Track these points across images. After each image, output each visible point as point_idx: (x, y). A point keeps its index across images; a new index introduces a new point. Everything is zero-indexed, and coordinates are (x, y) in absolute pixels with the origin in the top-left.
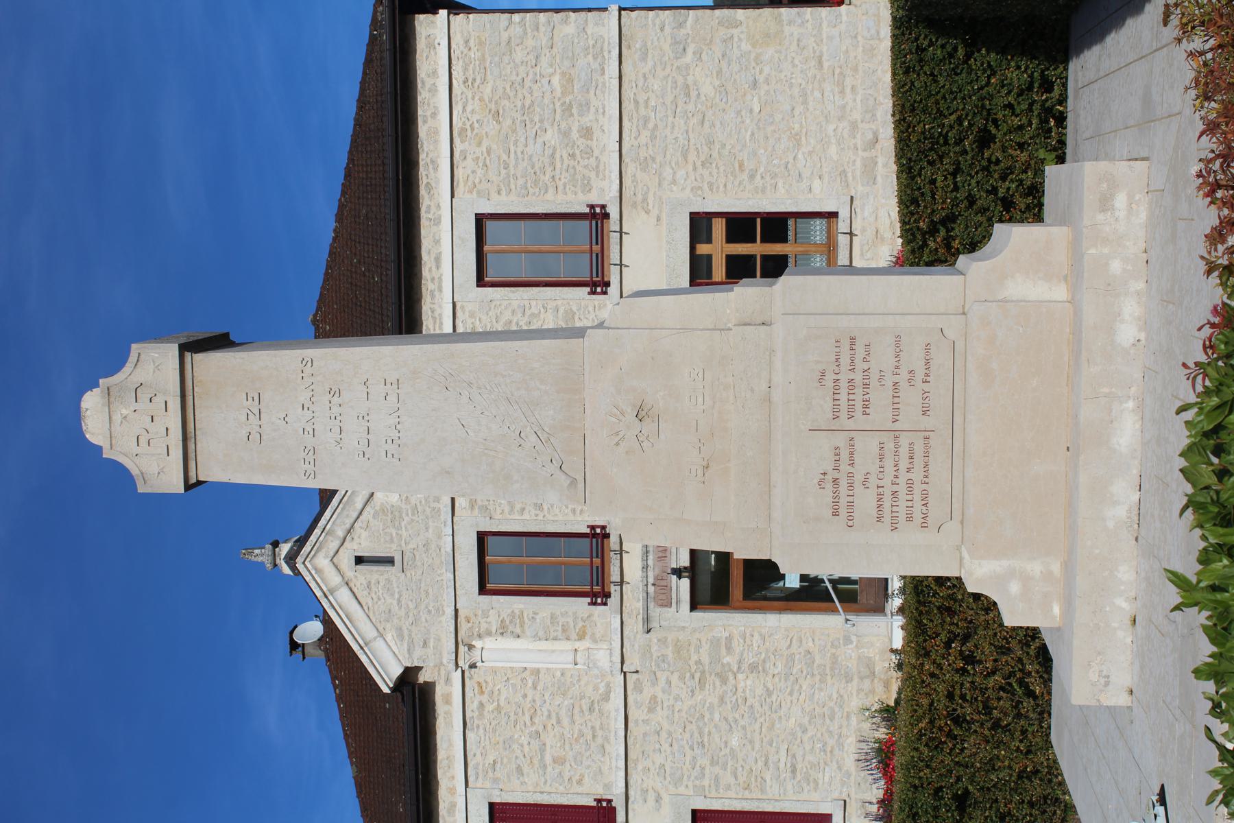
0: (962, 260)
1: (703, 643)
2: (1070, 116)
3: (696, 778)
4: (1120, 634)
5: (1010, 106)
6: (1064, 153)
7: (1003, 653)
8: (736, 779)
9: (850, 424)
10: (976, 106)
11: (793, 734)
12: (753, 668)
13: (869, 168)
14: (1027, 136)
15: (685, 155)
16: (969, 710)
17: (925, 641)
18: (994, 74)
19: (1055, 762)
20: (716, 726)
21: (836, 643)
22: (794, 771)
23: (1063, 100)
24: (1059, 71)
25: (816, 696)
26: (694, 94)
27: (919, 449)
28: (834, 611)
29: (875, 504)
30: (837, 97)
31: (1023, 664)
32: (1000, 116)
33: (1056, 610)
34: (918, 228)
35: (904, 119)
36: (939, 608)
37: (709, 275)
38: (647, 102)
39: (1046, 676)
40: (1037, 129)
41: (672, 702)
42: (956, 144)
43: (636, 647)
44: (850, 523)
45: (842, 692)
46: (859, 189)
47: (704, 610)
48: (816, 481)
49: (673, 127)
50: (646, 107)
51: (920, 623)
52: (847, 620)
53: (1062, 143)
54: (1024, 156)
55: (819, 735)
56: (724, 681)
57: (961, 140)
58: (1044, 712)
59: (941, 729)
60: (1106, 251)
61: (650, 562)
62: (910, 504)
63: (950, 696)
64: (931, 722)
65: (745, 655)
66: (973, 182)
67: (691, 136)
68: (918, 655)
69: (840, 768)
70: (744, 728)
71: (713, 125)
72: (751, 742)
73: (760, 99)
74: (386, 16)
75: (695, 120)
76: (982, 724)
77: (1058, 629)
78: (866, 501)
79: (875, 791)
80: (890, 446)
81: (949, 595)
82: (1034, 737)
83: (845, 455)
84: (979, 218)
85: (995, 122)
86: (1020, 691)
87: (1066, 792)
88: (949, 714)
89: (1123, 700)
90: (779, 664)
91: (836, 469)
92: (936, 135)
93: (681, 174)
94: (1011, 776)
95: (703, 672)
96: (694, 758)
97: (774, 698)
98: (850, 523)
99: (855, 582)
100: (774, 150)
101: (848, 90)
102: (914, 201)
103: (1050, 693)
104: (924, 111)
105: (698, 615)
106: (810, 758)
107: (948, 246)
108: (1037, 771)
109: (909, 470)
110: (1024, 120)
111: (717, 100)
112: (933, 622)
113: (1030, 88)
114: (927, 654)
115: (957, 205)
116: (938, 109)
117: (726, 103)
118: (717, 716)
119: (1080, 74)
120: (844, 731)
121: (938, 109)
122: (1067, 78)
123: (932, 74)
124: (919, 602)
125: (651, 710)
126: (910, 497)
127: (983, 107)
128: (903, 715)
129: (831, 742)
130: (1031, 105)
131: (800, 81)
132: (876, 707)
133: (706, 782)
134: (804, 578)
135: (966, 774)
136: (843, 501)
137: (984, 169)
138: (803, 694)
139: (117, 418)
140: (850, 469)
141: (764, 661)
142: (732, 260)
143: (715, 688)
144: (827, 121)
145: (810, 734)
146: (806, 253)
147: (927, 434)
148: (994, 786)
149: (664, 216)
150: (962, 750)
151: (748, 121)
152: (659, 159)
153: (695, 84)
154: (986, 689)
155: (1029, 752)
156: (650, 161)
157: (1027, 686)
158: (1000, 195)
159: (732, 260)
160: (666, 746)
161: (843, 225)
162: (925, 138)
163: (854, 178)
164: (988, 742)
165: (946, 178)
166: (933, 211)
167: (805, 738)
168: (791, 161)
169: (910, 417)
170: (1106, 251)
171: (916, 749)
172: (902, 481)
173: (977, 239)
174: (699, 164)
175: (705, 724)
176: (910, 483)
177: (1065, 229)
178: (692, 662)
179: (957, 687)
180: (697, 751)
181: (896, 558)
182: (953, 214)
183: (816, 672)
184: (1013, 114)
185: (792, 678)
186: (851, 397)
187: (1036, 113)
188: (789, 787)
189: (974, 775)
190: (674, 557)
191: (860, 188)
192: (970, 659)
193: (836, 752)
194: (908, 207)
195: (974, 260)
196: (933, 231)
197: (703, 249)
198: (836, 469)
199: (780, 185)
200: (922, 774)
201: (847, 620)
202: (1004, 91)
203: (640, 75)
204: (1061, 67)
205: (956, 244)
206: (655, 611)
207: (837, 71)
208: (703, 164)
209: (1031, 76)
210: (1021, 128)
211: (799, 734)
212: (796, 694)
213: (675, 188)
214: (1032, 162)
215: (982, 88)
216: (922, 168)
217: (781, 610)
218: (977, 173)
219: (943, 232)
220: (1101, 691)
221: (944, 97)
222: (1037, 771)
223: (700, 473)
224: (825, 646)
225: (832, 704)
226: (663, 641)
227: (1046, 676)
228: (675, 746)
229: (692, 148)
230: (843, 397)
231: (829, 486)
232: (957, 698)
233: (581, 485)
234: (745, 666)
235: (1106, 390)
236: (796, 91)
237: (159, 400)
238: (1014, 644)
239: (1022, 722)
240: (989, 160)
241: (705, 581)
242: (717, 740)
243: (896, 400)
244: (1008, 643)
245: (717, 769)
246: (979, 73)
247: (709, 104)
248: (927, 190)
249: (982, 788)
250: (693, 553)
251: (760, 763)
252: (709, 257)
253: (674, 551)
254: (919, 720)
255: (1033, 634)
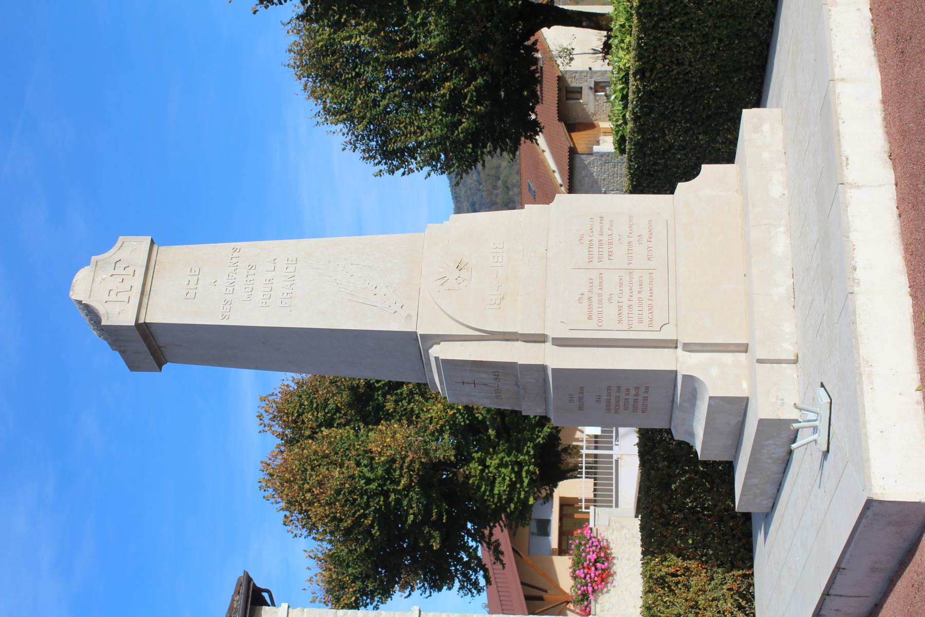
33: (745, 385)
48: (577, 298)
74: (241, 602)
80: (626, 278)
109: (639, 292)
136: (595, 310)
139: (98, 279)
176: (640, 300)
230: (595, 250)
231: (586, 302)
233: (414, 319)
237: (130, 271)
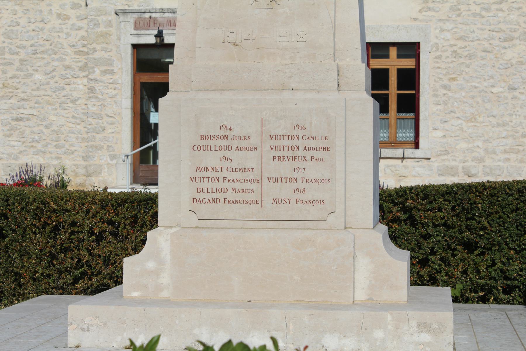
0: (385, 228)
1: (109, 54)
2: (486, 306)
3: (10, 49)
4: (119, 339)
5: (494, 264)
6: (459, 302)
7: (105, 261)
8: (11, 78)
9: (266, 148)
10: (494, 240)
11: (44, 119)
12: (92, 90)
13: (452, 171)
14: (472, 276)
15: (461, 38)
16: (63, 237)
17: (113, 206)
18: (517, 252)
19: (28, 298)
20: (48, 63)
21: (111, 149)
22: (18, 120)
23: (497, 301)
24: (519, 298)
25: (72, 135)
26: (506, 44)
27: (249, 196)
28: (134, 148)
29: (209, 165)
30: (501, 148)
31: (97, 275)
32: (487, 257)
33: (135, 294)
34: (407, 199)
35: (485, 189)
36: (136, 215)
37: (374, 57)
38: (501, 10)
39: (89, 291)
40: (477, 283)
41: (65, 31)
42: (467, 227)
43: (104, 5)
44: (195, 148)
45: (76, 154)
46: (435, 163)
47: (133, 54)
48: (225, 123)
49: (482, 29)
50: (497, 10)
51: (125, 202)
52: (127, 156)
53: (467, 301)
54: (457, 274)
55: (44, 137)
56: (82, 69)
57: (469, 230)
58: (63, 290)
59: (50, 217)
60: (390, 327)
61: (167, 15)
62: (210, 190)
63: (73, 224)
64: (54, 211)
65: (101, 84)
66: (440, 238)
67: (476, 43)
68: (102, 201)
69: (21, 152)
70: (48, 83)
71: (483, 58)
72: (38, 89)
73: (502, 92)
75: (487, 45)
76: (54, 247)
77: (122, 296)
78: (212, 159)
79: (5, 177)
80: (251, 176)
81: (145, 222)
82: (45, 283)
83: (244, 144)
84: (414, 242)
85: (483, 254)
86: (78, 273)
87: (6, 306)
88: (60, 223)
89: (72, 341)
90: (95, 108)
91: (234, 138)
92: (474, 212)
93: (448, 35)
94: (17, 268)
95: (88, 53)
96: (25, 47)
97: (70, 105)
98: (195, 148)
99: (155, 162)
100: (464, 103)
101: (507, 156)
102: (426, 197)
103: (76, 294)
104: (491, 203)
105: (129, 50)
106: (28, 131)
107: (394, 221)
108: (21, 286)
109: (234, 190)
110: (483, 274)
111: (502, 62)
112: (126, 211)
113: (507, 278)
114: (103, 207)
115: (423, 227)
116: (492, 213)
117: (499, 68)
118: (56, 64)
119: (516, 313)
120: (48, 155)
121: (492, 213)
122: (513, 304)
123: (517, 209)
124: (140, 201)
125: (59, 16)
126: (214, 190)
127: (494, 245)
128: (59, 192)
129: (39, 146)
130: (494, 279)
131: (514, 121)
132: (66, 178)
133: (7, 56)
134: (156, 125)
135: (18, 236)
136: (211, 143)
137: (449, 246)
138: (74, 126)
140: (234, 148)
141: (97, 97)
142: (385, 72)
143: (77, 62)
144: (484, 141)
145: (45, 131)
146: (389, 126)
147: (260, 202)
148: (9, 256)
149: (417, 23)
150: (35, 233)
151: (485, 84)
152: (459, 19)
153: (514, 45)
154: (79, 249)
155: (34, 280)
156: (457, 12)
157: (81, 278)
158: (430, 257)
159: (385, 72)
160: (33, 27)
161: (409, 152)
162: (471, 204)
163: (443, 160)
164: (41, 251)
165: (442, 219)
166: (419, 210)
167: (42, 128)
168: (456, 115)
169: (272, 190)
170: (390, 327)
171: (34, 200)
172: (226, 185)
173: (399, 241)
174: (455, 48)
175: (50, 55)
177: (406, 299)
178: (95, 45)
179: (80, 229)
180: (30, 50)
181: (172, 190)
182: (417, 225)
183: (90, 135)
184: (488, 266)
185: (85, 118)
186: (286, 148)
187: (488, 282)
188: (6, 116)
189: (17, 241)
190: (170, 32)
191: (436, 165)
192: (100, 238)
193: (32, 150)
194: (422, 192)
195: (383, 235)
196: (405, 210)
197: (393, 52)
198: (234, 138)
199: (439, 107)
200: (17, 205)
201: (127, 156)
202: (505, 260)
203: (521, 5)
204: (521, 300)
205: (395, 226)
206: (131, 19)
207: (521, 148)
208: (455, 52)
209: (515, 279)
210: (478, 272)
211: (44, 123)
212: (73, 120)
213: (437, 31)
214: (453, 280)
215: (507, 244)
216: (450, 202)
217: (134, 109)
218: (446, 241)
219: (404, 217)
220: (78, 326)
221: (501, 217)
222: (21, 286)
223: (231, 40)
224: (108, 141)
225: (67, 146)
226: (109, 24)
227: (89, 291)
228: (33, 34)
229: (466, 44)
231: (222, 133)
232: (72, 228)
234: (92, 84)
235: (291, 327)
236: (507, 119)
238: (112, 268)
239: (55, 275)
240: (455, 249)
241: (154, 55)
242: (39, 64)
243: (284, 180)
244: (112, 264)
245: (17, 64)
246: (518, 242)
247: (498, 56)
248: (434, 205)
249: (8, 248)
250: (172, 46)
251: (22, 95)
252: (387, 56)
253: (174, 32)
254: (56, 202)
255: (118, 281)
